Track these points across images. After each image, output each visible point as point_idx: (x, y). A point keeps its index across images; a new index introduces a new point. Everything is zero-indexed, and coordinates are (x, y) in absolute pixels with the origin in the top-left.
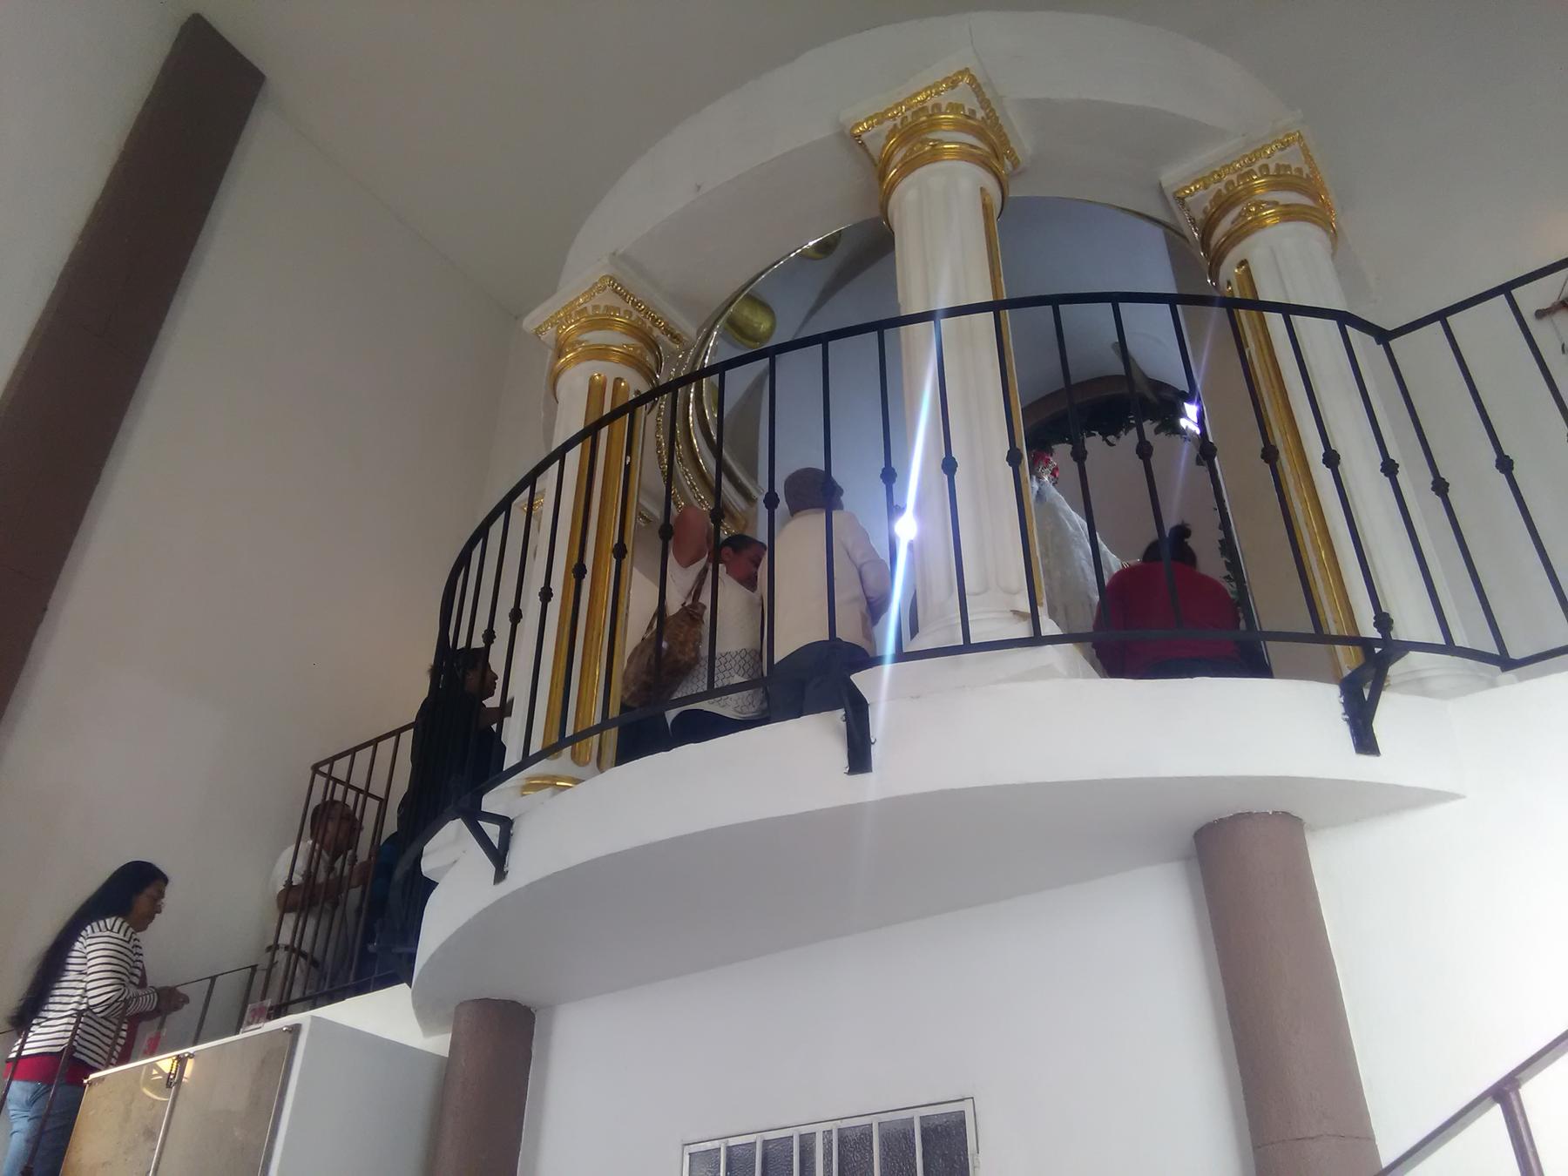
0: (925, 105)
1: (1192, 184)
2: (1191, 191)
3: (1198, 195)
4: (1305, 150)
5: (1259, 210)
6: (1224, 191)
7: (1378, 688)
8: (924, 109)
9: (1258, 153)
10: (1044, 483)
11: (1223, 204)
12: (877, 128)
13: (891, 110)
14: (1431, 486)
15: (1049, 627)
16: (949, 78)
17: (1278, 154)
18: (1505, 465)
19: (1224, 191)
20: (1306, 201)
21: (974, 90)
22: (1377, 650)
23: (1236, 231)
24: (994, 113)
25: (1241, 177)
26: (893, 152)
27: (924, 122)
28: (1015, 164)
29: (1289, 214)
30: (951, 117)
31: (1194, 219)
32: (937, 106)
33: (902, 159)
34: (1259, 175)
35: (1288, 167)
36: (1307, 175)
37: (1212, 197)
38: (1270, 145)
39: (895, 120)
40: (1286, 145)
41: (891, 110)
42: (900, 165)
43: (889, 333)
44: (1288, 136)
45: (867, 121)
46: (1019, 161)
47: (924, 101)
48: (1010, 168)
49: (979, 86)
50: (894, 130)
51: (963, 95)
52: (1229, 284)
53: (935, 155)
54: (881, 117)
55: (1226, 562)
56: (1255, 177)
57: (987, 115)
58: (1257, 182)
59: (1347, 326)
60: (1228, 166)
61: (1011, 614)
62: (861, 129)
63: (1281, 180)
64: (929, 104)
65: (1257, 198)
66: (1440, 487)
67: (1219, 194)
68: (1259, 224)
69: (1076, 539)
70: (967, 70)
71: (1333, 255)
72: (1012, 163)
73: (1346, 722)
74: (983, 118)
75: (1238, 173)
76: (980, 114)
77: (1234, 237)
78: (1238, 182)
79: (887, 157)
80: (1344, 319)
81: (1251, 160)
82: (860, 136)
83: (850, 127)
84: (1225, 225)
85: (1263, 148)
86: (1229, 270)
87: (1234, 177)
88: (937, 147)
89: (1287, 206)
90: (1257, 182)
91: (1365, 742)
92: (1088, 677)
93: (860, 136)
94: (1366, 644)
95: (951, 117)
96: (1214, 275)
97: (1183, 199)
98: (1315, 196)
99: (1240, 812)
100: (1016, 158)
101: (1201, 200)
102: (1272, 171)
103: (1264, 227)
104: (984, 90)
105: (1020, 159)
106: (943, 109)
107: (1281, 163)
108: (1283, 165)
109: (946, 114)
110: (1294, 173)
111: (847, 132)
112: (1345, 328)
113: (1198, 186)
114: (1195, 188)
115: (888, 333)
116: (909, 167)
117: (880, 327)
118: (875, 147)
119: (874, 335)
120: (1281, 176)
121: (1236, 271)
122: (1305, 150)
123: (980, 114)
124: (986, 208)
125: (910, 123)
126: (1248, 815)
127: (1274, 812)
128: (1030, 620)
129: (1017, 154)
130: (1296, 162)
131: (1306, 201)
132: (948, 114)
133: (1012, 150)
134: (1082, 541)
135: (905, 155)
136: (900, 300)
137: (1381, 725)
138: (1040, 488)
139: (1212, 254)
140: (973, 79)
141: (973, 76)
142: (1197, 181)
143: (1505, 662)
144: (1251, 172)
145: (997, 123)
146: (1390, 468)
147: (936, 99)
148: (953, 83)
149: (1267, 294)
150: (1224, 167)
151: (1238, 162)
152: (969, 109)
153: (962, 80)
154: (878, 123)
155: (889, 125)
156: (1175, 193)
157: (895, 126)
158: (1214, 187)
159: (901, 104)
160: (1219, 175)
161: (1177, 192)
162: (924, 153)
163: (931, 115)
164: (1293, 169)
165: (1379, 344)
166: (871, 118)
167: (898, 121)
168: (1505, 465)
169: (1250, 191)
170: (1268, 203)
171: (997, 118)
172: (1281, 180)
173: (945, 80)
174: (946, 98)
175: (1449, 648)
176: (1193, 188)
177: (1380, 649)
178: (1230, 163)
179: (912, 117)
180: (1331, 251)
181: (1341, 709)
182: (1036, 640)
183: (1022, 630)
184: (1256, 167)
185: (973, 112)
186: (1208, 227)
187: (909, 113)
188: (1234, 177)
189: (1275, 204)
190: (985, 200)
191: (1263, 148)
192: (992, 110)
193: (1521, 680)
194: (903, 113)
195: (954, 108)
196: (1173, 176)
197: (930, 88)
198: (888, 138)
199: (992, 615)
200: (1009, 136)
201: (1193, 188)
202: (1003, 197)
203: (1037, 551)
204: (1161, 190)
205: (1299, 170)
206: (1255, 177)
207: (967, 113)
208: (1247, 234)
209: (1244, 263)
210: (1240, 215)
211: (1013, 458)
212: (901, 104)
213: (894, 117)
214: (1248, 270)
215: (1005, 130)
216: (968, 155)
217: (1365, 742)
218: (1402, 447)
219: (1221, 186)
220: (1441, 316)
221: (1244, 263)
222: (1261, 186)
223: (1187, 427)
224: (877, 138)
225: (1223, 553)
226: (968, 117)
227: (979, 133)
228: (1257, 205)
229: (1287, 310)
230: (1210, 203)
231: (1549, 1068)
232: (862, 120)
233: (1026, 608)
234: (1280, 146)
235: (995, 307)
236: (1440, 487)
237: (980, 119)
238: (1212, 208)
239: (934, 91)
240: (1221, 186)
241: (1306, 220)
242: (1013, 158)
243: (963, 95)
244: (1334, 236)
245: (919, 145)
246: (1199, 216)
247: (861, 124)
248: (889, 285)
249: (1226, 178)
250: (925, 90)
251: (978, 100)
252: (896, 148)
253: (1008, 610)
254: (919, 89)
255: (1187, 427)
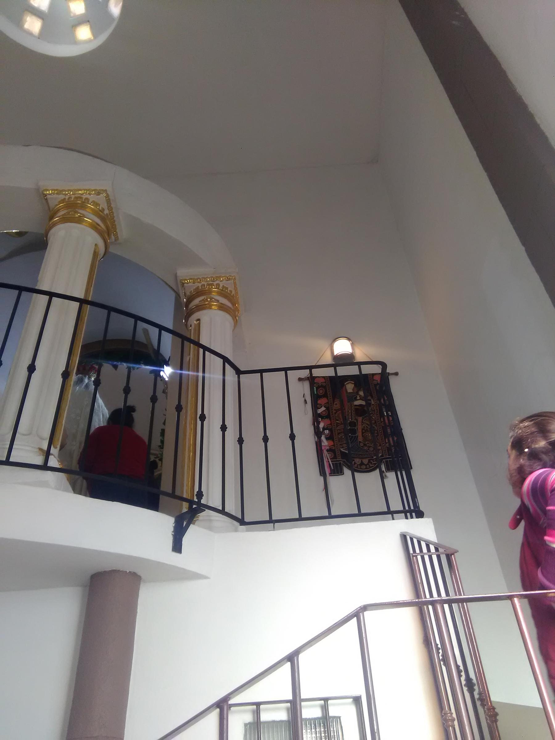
0: (82, 196)
1: (188, 279)
2: (187, 281)
3: (190, 284)
4: (235, 284)
5: (211, 301)
6: (200, 288)
7: (191, 521)
8: (81, 198)
9: (218, 277)
10: (91, 380)
11: (199, 293)
12: (55, 196)
13: (65, 191)
14: (238, 439)
15: (53, 462)
16: (97, 190)
17: (224, 281)
18: (266, 439)
19: (200, 288)
20: (229, 304)
21: (107, 200)
22: (194, 506)
23: (201, 305)
24: (113, 214)
25: (209, 285)
26: (59, 210)
27: (79, 203)
28: (117, 239)
29: (222, 307)
30: (92, 207)
31: (186, 294)
32: (87, 199)
33: (63, 215)
34: (215, 287)
35: (227, 288)
36: (233, 295)
37: (195, 288)
38: (223, 277)
39: (66, 196)
40: (228, 279)
41: (65, 191)
42: (61, 217)
43: (25, 295)
44: (230, 276)
45: (52, 190)
46: (118, 239)
47: (82, 194)
48: (114, 240)
49: (109, 199)
50: (63, 201)
51: (101, 199)
52: (191, 326)
53: (79, 221)
54: (60, 192)
55: (161, 439)
56: (213, 287)
57: (110, 213)
58: (213, 289)
59: (226, 363)
60: (205, 278)
61: (38, 450)
62: (48, 192)
63: (223, 293)
64: (84, 197)
65: (212, 296)
66: (241, 441)
67: (198, 288)
68: (210, 307)
69: (97, 411)
70: (106, 191)
71: (233, 330)
72: (115, 238)
73: (172, 536)
74: (107, 213)
75: (207, 283)
76: (106, 212)
77: (199, 308)
78: (207, 287)
79: (57, 210)
80: (226, 360)
81: (214, 279)
82: (46, 195)
83: (43, 190)
84: (196, 301)
85: (220, 277)
86: (193, 320)
87: (206, 284)
88: (81, 217)
89: (222, 303)
90: (213, 289)
91: (177, 547)
92: (65, 490)
93: (46, 195)
94: (191, 502)
95: (92, 207)
96: (187, 318)
97: (183, 284)
98: (234, 304)
99: (115, 569)
100: (118, 237)
101: (191, 287)
102: (221, 288)
103: (211, 309)
104: (111, 202)
105: (119, 237)
106: (90, 202)
107: (225, 286)
108: (225, 287)
109: (90, 204)
110: (228, 292)
111: (41, 191)
112: (225, 363)
113: (191, 281)
114: (190, 281)
115: (24, 294)
116: (65, 220)
117: (21, 289)
118: (52, 204)
119: (17, 292)
120: (223, 291)
121: (195, 322)
122: (235, 284)
123: (106, 212)
124: (95, 254)
125: (72, 201)
126: (114, 572)
127: (129, 572)
128: (45, 456)
129: (118, 235)
130: (231, 288)
131: (229, 304)
132: (91, 205)
133: (117, 233)
134: (99, 413)
135: (65, 214)
136: (39, 278)
137: (186, 540)
138: (88, 382)
139: (188, 311)
140: (108, 196)
141: (108, 194)
142: (191, 279)
143: (242, 522)
144: (212, 285)
145: (113, 218)
146: (224, 428)
147: (88, 196)
148: (98, 193)
149: (204, 341)
150: (203, 278)
151: (209, 278)
152: (102, 207)
153: (102, 194)
154: (57, 194)
155: (62, 197)
156: (181, 280)
157: (65, 199)
158: (197, 284)
159: (71, 191)
160: (200, 280)
161: (182, 280)
162: (74, 217)
163: (83, 202)
164: (229, 289)
165: (236, 374)
166: (54, 190)
167: (67, 197)
168: (266, 439)
169: (210, 292)
170: (215, 300)
171: (114, 217)
172: (223, 293)
173: (95, 190)
174: (92, 198)
175: (223, 512)
176: (188, 281)
177: (196, 506)
178: (206, 277)
179: (74, 199)
180: (233, 328)
181: (172, 529)
182: (45, 467)
183: (38, 460)
184: (215, 283)
185: (103, 210)
186: (190, 300)
187: (73, 196)
188: (206, 284)
189: (218, 301)
190: (96, 249)
191: (220, 277)
192: (112, 212)
193: (247, 530)
194: (70, 195)
195: (96, 204)
196: (183, 272)
197: (87, 190)
198: (60, 203)
199: (27, 448)
200: (117, 227)
201: (188, 281)
202: (106, 250)
203: (63, 421)
204: (176, 276)
205: (231, 291)
206: (213, 287)
207: (100, 208)
208: (204, 309)
209: (199, 320)
210: (203, 300)
211: (66, 375)
212: (71, 191)
213: (66, 195)
214: (199, 324)
215: (116, 223)
216: (94, 227)
217: (177, 547)
218: (231, 422)
219: (200, 285)
220: (261, 372)
221: (199, 320)
222: (214, 292)
223: (162, 376)
224: (54, 200)
225: (161, 436)
226: (100, 211)
227: (103, 219)
228: (211, 299)
229: (206, 349)
230: (194, 289)
231: (233, 689)
232: (50, 189)
233: (45, 447)
234: (226, 279)
235: (82, 302)
236: (241, 441)
237: (106, 214)
238: (194, 292)
239: (88, 192)
240: (200, 285)
241: (227, 312)
242: (116, 236)
243: (101, 199)
244: (236, 322)
245: (73, 213)
246: (188, 293)
247: (49, 190)
248: (36, 269)
249: (203, 283)
250: (84, 190)
251: (107, 205)
252: (62, 208)
253: (37, 447)
254: (66, 189)
255: (162, 376)
